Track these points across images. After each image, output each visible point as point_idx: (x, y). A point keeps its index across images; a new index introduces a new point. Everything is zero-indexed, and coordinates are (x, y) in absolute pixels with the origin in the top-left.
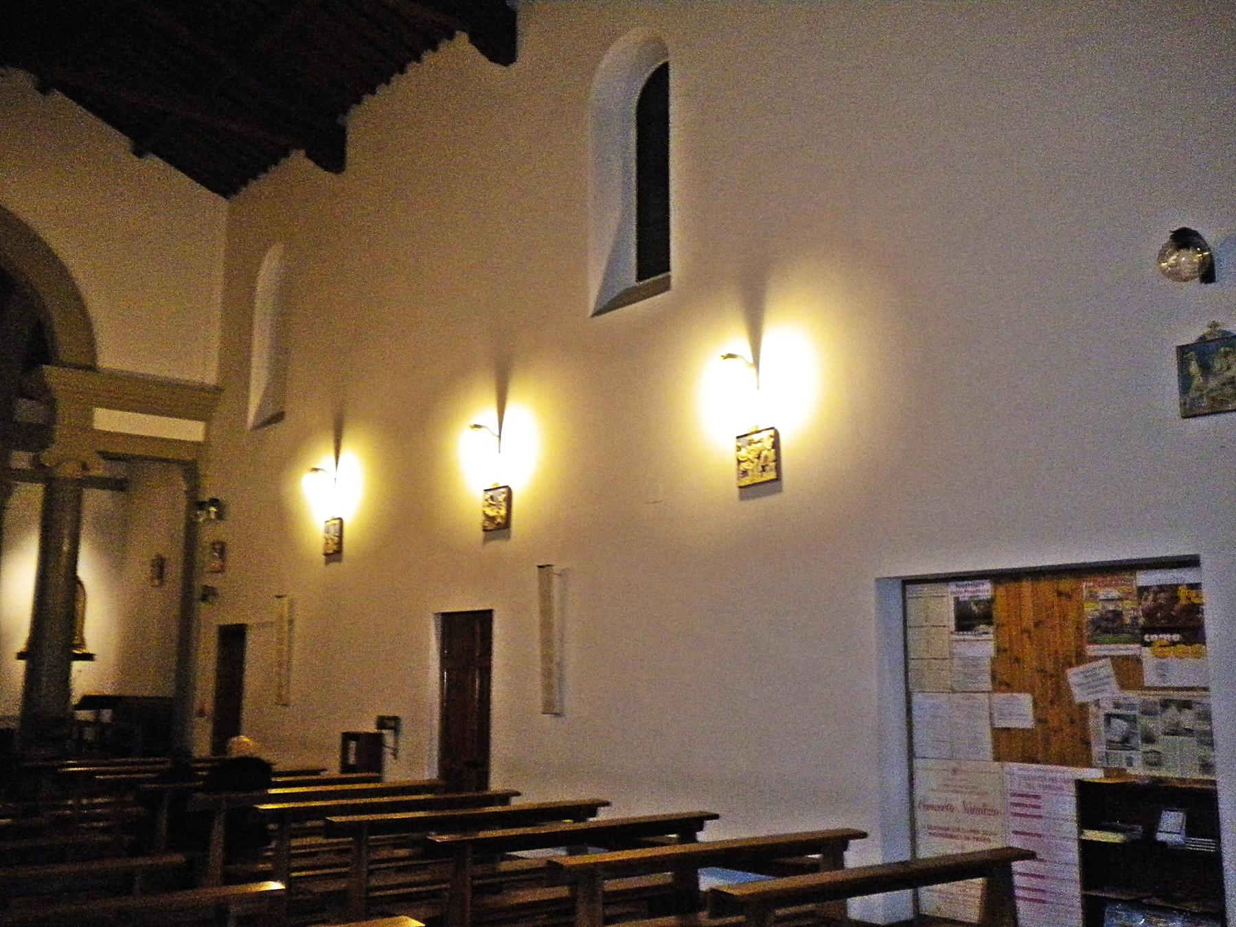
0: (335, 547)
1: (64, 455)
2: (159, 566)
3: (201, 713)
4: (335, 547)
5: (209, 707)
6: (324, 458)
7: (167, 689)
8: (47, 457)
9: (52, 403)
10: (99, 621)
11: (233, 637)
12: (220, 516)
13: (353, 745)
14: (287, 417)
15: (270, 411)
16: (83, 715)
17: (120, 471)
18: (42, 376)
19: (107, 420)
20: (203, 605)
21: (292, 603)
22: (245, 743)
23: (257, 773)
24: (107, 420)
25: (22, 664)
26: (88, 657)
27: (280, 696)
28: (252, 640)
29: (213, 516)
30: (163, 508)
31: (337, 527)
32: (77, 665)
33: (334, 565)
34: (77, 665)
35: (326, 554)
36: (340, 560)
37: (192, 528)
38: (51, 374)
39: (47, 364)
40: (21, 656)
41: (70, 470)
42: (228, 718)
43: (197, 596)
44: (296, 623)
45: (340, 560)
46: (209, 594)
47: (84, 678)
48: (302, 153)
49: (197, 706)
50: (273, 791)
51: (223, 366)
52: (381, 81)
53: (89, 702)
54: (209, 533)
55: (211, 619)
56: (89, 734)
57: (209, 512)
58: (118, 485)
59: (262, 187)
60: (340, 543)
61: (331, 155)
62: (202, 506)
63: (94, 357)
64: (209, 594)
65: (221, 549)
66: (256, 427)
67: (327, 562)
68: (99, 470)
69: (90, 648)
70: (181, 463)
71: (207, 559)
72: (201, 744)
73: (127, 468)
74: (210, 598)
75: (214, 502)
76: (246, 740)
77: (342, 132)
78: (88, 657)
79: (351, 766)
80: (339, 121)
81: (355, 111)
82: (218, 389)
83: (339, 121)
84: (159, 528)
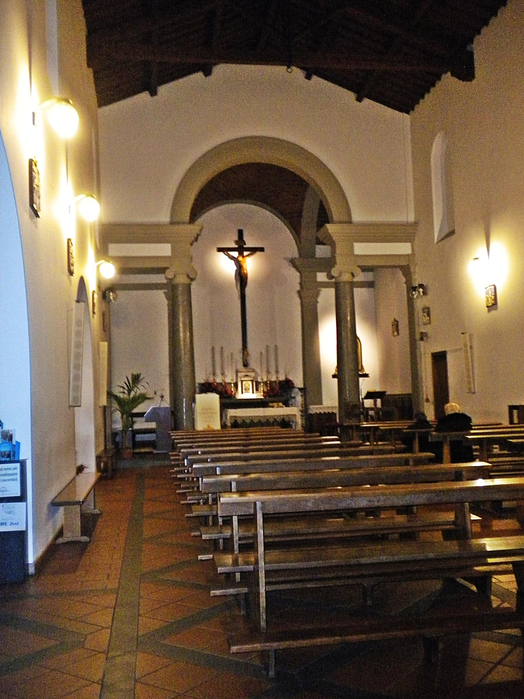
0: (493, 302)
1: (342, 270)
2: (396, 325)
3: (427, 400)
4: (493, 302)
5: (431, 398)
6: (479, 249)
7: (409, 390)
8: (334, 272)
9: (333, 245)
10: (370, 356)
11: (440, 359)
12: (425, 293)
13: (515, 412)
14: (456, 231)
15: (446, 231)
16: (368, 403)
17: (369, 276)
18: (327, 230)
19: (360, 249)
20: (421, 342)
21: (471, 336)
22: (453, 406)
23: (462, 421)
24: (360, 249)
25: (336, 380)
26: (366, 375)
27: (470, 389)
28: (450, 358)
29: (421, 294)
30: (395, 287)
31: (493, 290)
32: (361, 379)
33: (493, 312)
34: (361, 379)
35: (488, 307)
36: (496, 309)
37: (410, 301)
38: (330, 227)
39: (328, 223)
40: (334, 376)
41: (346, 277)
42: (442, 394)
43: (418, 337)
44: (474, 347)
45: (496, 309)
46: (423, 336)
47: (365, 386)
48: (449, 74)
49: (425, 397)
50: (472, 432)
51: (417, 211)
52: (491, 15)
53: (370, 395)
54: (420, 304)
55: (427, 351)
56: (371, 413)
57: (419, 292)
58: (370, 285)
59: (427, 104)
60: (495, 299)
61: (466, 72)
62: (414, 289)
63: (350, 215)
64: (423, 336)
65: (427, 311)
66: (437, 243)
67: (489, 311)
68: (361, 277)
69: (366, 371)
70: (402, 267)
71: (420, 317)
72: (430, 413)
73: (374, 271)
74: (425, 338)
75: (421, 286)
76: (453, 404)
77: (471, 54)
78: (366, 375)
79: (517, 409)
80: (469, 48)
81: (478, 39)
82: (416, 224)
83: (469, 48)
84: (395, 308)
